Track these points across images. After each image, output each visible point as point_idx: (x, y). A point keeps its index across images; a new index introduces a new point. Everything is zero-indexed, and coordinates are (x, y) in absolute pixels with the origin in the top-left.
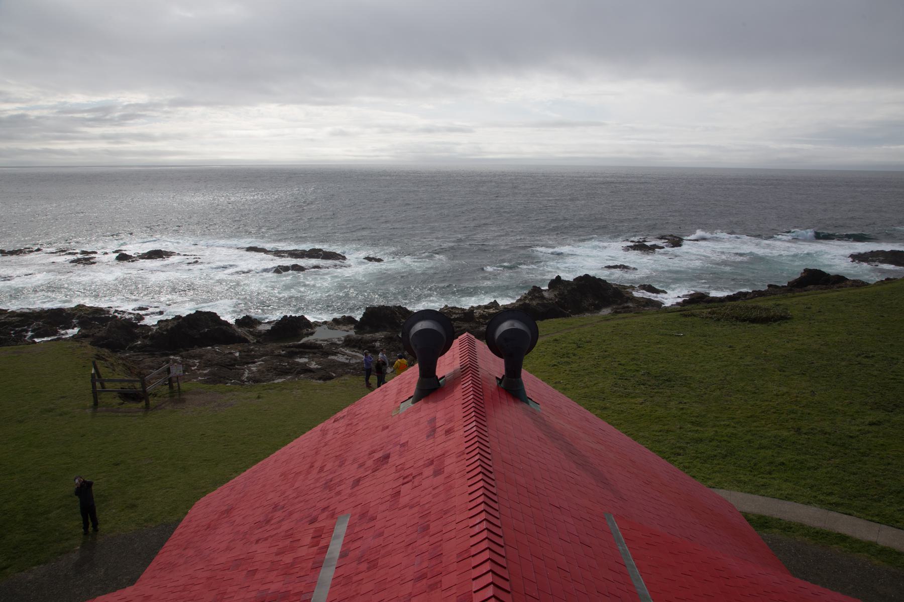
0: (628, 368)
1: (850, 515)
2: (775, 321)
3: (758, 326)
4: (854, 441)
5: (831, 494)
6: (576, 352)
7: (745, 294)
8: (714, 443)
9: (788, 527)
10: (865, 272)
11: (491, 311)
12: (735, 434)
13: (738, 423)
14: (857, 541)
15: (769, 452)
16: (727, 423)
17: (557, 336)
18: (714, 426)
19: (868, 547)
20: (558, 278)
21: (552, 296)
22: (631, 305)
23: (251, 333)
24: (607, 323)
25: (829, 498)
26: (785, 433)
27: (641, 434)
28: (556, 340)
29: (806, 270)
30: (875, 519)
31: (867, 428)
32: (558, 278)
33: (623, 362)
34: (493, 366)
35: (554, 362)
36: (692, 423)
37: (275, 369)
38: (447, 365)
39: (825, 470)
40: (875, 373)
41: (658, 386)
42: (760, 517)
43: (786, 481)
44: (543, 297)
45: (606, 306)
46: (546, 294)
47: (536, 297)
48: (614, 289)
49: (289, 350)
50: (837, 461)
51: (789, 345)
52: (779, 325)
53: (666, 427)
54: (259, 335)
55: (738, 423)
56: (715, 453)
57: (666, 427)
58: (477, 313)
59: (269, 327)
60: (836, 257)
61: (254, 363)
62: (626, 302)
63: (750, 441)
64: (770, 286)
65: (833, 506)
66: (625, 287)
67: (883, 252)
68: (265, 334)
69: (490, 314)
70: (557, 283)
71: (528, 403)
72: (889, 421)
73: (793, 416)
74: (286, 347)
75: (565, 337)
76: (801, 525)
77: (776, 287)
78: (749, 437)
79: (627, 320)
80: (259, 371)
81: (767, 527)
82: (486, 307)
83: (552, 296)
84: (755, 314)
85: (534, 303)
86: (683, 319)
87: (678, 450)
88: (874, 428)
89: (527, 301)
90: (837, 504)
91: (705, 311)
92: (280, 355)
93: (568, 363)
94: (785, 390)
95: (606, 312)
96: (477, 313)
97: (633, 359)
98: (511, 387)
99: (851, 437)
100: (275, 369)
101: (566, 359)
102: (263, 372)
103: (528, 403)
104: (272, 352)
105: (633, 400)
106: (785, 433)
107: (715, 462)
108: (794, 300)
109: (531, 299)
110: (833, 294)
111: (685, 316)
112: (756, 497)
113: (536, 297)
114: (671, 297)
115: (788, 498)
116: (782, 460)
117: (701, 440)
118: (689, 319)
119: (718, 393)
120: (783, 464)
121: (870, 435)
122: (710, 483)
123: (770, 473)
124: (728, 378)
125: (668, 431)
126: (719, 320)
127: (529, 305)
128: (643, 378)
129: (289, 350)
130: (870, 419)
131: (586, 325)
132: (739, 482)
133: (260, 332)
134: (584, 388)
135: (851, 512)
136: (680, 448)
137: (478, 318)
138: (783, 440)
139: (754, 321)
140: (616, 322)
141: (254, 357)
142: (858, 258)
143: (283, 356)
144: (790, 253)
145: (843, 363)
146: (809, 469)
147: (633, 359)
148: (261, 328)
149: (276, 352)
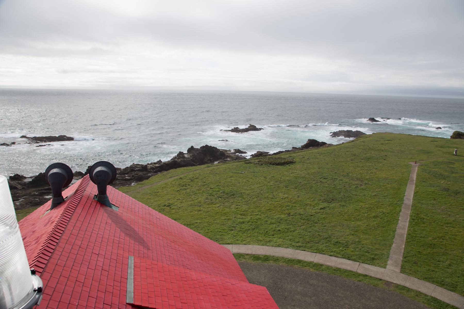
0: (214, 190)
1: (304, 251)
2: (288, 164)
3: (280, 167)
4: (312, 217)
5: (298, 242)
6: (190, 183)
7: (282, 152)
8: (250, 223)
9: (276, 259)
10: (335, 141)
11: (157, 165)
12: (260, 218)
13: (262, 213)
14: (305, 262)
15: (274, 226)
16: (257, 213)
17: (182, 176)
18: (251, 215)
19: (309, 264)
20: (192, 147)
21: (189, 156)
22: (229, 159)
23: (19, 184)
24: (208, 168)
25: (297, 244)
26: (283, 216)
27: (215, 222)
28: (181, 178)
29: (309, 140)
30: (315, 251)
31: (318, 211)
32: (192, 147)
33: (212, 187)
34: (92, 189)
35: (178, 189)
36: (241, 215)
37: (31, 203)
38: (67, 193)
39: (297, 232)
40: (327, 186)
41: (227, 198)
42: (265, 256)
43: (280, 238)
44: (184, 157)
45: (216, 160)
46: (186, 156)
47: (181, 157)
48: (220, 151)
49: (40, 192)
50: (304, 227)
51: (292, 175)
52: (289, 166)
53: (228, 217)
54: (25, 184)
55: (262, 213)
56: (249, 228)
57: (228, 217)
58: (149, 167)
59: (31, 180)
60: (323, 135)
61: (18, 200)
62: (227, 158)
63: (266, 221)
64: (293, 148)
65: (298, 248)
66: (226, 151)
67: (344, 131)
68: (28, 184)
69: (156, 167)
70: (191, 149)
71: (111, 207)
72: (328, 207)
73: (288, 208)
74: (39, 190)
75: (186, 176)
76: (283, 258)
77: (296, 148)
78: (266, 219)
79: (218, 167)
80: (21, 204)
81: (267, 260)
82: (155, 163)
83: (189, 156)
84: (279, 161)
85: (180, 160)
86: (246, 165)
87: (232, 228)
88: (322, 211)
89: (176, 160)
90: (300, 247)
91: (256, 161)
92: (35, 195)
93: (186, 189)
94: (286, 196)
95: (216, 163)
96: (149, 167)
97: (218, 186)
98: (102, 200)
99: (312, 215)
100: (31, 203)
101: (184, 188)
102: (23, 205)
103: (111, 207)
104: (30, 193)
105: (214, 206)
106: (283, 216)
107: (249, 232)
108: (298, 154)
109: (178, 158)
110: (321, 149)
111: (246, 163)
112: (264, 247)
113: (181, 157)
114: (248, 155)
115: (279, 246)
116: (279, 228)
117: (244, 222)
118: (248, 165)
119: (255, 199)
120: (279, 230)
121: (319, 214)
122: (244, 242)
123: (273, 235)
124: (262, 192)
125: (228, 219)
126: (262, 165)
127: (176, 161)
128: (221, 194)
129: (40, 192)
130: (321, 207)
131: (198, 170)
132: (258, 241)
133: (25, 183)
134: (191, 201)
135: (305, 249)
136: (233, 227)
137: (150, 169)
138: (281, 220)
139: (278, 164)
140: (212, 168)
141: (19, 197)
142: (335, 134)
143: (37, 195)
144: (302, 136)
145: (314, 182)
146: (291, 232)
147: (218, 186)
148: (26, 180)
149: (32, 193)
